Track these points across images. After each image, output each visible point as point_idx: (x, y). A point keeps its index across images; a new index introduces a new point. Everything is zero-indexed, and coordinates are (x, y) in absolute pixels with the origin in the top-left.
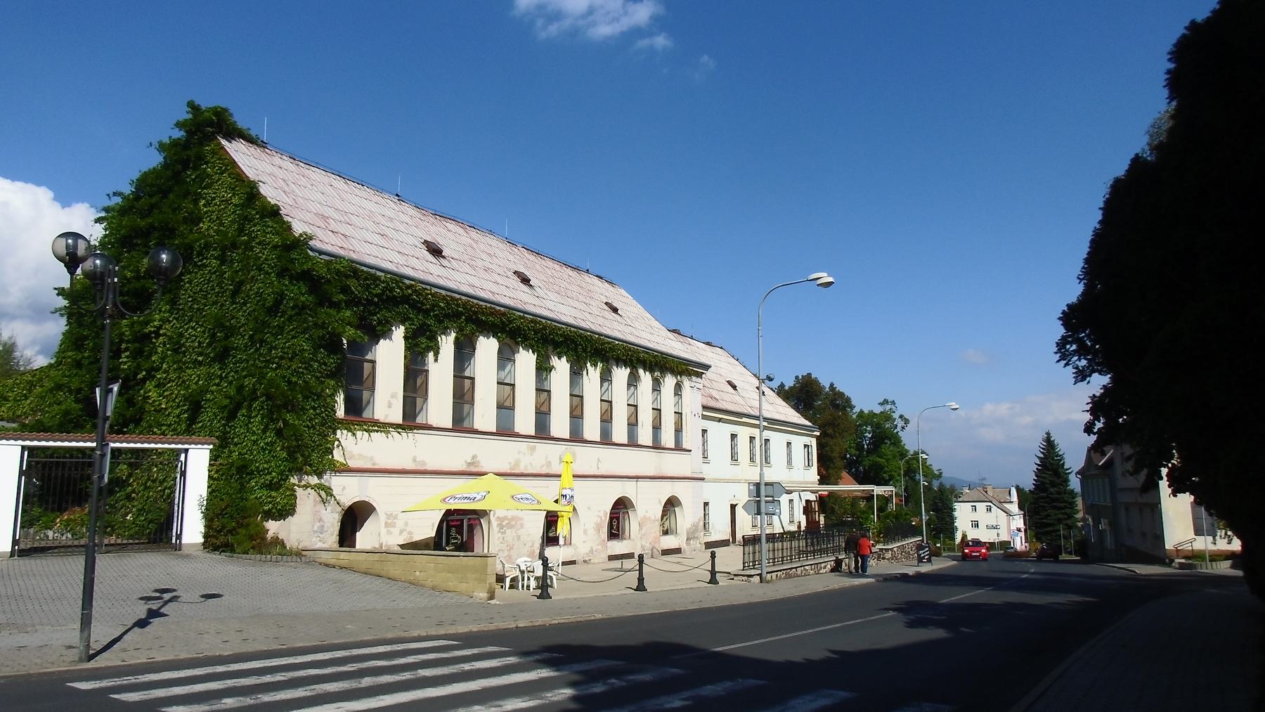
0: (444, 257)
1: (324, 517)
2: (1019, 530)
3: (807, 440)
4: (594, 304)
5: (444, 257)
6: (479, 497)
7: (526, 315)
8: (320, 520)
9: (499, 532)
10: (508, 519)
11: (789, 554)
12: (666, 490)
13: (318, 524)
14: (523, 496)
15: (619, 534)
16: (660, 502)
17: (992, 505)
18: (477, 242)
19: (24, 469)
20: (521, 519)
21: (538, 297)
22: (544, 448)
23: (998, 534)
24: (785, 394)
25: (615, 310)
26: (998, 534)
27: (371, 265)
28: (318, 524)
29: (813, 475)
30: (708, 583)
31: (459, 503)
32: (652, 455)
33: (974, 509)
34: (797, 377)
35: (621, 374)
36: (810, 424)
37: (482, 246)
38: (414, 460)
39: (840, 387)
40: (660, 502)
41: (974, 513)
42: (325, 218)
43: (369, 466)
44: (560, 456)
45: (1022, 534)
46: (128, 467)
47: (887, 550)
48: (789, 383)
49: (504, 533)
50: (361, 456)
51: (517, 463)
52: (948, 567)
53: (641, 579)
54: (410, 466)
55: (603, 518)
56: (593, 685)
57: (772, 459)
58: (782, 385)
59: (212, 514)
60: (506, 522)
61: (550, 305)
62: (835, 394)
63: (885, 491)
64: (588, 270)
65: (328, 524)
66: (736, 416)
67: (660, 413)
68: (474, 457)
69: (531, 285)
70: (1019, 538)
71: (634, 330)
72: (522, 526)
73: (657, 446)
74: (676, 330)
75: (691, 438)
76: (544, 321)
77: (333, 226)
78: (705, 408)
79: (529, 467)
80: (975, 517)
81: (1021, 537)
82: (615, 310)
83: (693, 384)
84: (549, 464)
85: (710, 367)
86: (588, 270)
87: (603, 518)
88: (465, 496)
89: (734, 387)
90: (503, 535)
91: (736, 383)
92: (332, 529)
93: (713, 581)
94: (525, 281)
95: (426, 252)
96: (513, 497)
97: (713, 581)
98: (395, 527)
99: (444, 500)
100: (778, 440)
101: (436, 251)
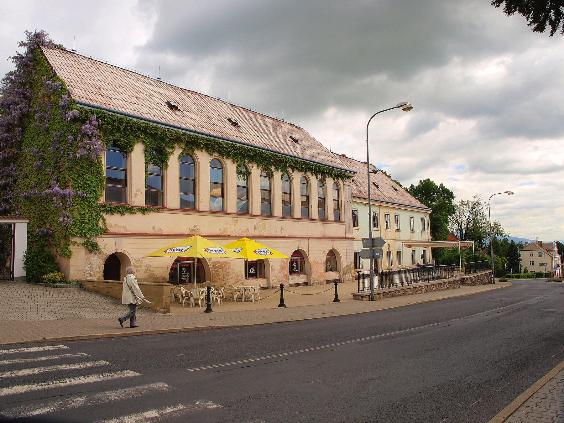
0: (179, 110)
1: (93, 262)
2: (558, 266)
3: (424, 216)
4: (282, 137)
5: (179, 110)
6: (185, 249)
7: (233, 143)
8: (90, 263)
12: (327, 246)
13: (89, 266)
14: (262, 250)
16: (324, 252)
17: (542, 252)
20: (229, 263)
22: (268, 222)
23: (546, 269)
25: (296, 141)
26: (546, 269)
27: (87, 105)
28: (89, 266)
29: (427, 236)
33: (531, 255)
35: (297, 176)
37: (210, 106)
38: (154, 228)
39: (446, 186)
40: (324, 252)
41: (531, 257)
42: (100, 88)
43: (123, 231)
44: (255, 225)
45: (560, 268)
46: (479, 257)
47: (467, 278)
50: (117, 226)
54: (151, 231)
55: (286, 262)
56: (104, 392)
57: (402, 227)
59: (29, 260)
60: (218, 264)
62: (443, 191)
63: (468, 245)
64: (283, 120)
67: (324, 200)
68: (195, 226)
70: (558, 270)
71: (307, 152)
72: (230, 267)
73: (323, 218)
74: (343, 155)
75: (347, 216)
76: (105, 112)
77: (104, 92)
79: (234, 232)
80: (532, 259)
81: (559, 270)
82: (296, 141)
86: (283, 120)
87: (286, 262)
90: (217, 273)
94: (235, 124)
99: (166, 251)
100: (404, 216)
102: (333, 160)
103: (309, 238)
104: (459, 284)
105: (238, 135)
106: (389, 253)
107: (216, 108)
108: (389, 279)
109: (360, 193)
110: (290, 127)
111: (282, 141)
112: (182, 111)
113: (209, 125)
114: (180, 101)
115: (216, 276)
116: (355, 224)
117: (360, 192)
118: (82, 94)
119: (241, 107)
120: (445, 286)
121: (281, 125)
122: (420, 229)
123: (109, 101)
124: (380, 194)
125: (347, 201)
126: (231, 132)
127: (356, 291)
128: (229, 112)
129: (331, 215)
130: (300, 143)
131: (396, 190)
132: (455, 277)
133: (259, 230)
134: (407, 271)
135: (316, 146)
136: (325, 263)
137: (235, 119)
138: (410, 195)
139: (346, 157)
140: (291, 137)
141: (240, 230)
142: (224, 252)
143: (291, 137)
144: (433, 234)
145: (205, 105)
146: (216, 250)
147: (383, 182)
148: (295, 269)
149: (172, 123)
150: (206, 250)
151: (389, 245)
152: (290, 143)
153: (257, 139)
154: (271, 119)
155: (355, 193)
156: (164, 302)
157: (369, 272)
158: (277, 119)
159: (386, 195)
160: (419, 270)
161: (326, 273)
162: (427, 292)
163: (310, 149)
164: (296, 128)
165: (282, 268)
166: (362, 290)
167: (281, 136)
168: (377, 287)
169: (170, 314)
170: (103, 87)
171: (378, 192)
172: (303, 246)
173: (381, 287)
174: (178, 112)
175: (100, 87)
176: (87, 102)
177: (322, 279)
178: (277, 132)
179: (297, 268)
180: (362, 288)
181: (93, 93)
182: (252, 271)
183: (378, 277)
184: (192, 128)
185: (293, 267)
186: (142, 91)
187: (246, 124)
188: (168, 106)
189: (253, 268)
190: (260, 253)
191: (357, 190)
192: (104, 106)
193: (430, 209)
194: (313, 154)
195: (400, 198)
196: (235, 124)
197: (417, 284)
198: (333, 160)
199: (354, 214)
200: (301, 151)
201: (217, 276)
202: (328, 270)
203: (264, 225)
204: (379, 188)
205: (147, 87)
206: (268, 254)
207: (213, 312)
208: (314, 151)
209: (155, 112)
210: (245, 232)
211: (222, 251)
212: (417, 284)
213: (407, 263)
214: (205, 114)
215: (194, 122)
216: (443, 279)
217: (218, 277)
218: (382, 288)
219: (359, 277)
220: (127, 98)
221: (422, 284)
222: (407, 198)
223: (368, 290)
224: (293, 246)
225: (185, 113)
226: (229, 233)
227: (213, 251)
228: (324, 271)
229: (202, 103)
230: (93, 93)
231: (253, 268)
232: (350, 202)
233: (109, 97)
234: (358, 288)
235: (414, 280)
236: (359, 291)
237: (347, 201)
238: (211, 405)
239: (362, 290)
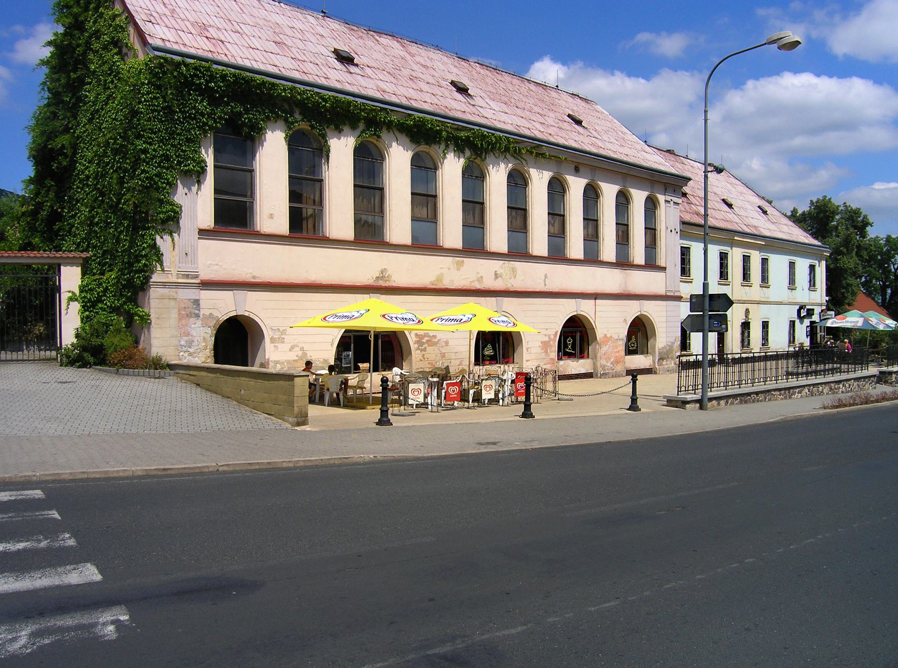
0: (357, 65)
5: (357, 65)
6: (465, 319)
9: (418, 349)
10: (429, 336)
11: (762, 376)
15: (575, 353)
18: (412, 55)
19: (58, 294)
21: (473, 105)
22: (521, 266)
24: (797, 219)
25: (579, 122)
30: (628, 409)
31: (450, 325)
32: (617, 273)
34: (811, 201)
36: (820, 244)
37: (418, 59)
42: (204, 27)
47: (891, 373)
48: (803, 208)
49: (425, 350)
51: (440, 278)
52: (45, 589)
53: (634, 399)
57: (807, 271)
58: (794, 211)
60: (427, 339)
61: (488, 113)
64: (557, 86)
65: (199, 339)
66: (729, 236)
69: (469, 95)
71: (597, 141)
73: (623, 262)
74: (670, 150)
77: (213, 32)
78: (684, 223)
82: (579, 122)
83: (669, 198)
84: (480, 279)
85: (690, 179)
86: (557, 86)
88: (452, 318)
89: (730, 206)
90: (423, 353)
91: (730, 200)
92: (204, 344)
93: (634, 407)
94: (462, 90)
95: (336, 61)
96: (489, 319)
97: (634, 407)
98: (283, 342)
100: (778, 263)
101: (345, 59)
102: (648, 156)
103: (596, 296)
104: (873, 383)
105: (467, 110)
106: (746, 326)
107: (429, 64)
108: (740, 372)
109: (696, 216)
110: (570, 99)
111: (550, 121)
112: (362, 66)
113: (411, 91)
114: (359, 50)
115: (422, 359)
116: (685, 271)
117: (697, 215)
118: (170, 35)
119: (478, 63)
120: (847, 386)
121: (554, 94)
122: (806, 285)
123: (221, 49)
124: (736, 219)
125: (671, 231)
126: (455, 105)
127: (672, 392)
128: (455, 70)
129: (638, 254)
130: (585, 126)
131: (765, 212)
132: (868, 369)
133: (503, 279)
134: (777, 357)
135: (618, 131)
136: (625, 339)
137: (465, 81)
138: (791, 223)
139: (674, 154)
140: (569, 116)
141: (468, 278)
142: (419, 321)
143: (569, 116)
144: (830, 290)
145: (408, 57)
146: (403, 318)
147: (742, 198)
148: (570, 349)
149: (338, 86)
150: (384, 316)
151: (746, 310)
152: (566, 126)
153: (504, 117)
154: (533, 83)
155: (687, 218)
156: (295, 405)
157: (700, 358)
158: (547, 85)
159: (748, 221)
160: (799, 355)
161: (626, 357)
162: (812, 395)
163: (605, 138)
164: (580, 101)
165: (545, 345)
166: (717, 387)
167: (552, 115)
168: (744, 382)
169: (306, 428)
170: (212, 23)
171: (730, 216)
172: (585, 308)
173: (736, 383)
174: (353, 69)
175: (207, 23)
176: (176, 47)
177: (619, 368)
178: (544, 106)
179: (574, 348)
180: (685, 387)
181: (191, 33)
182: (489, 351)
183: (725, 366)
184: (378, 95)
185: (566, 346)
186: (289, 32)
187: (485, 92)
188: (335, 58)
189: (489, 346)
190: (497, 322)
191: (691, 211)
192: (210, 55)
193: (827, 248)
194: (610, 146)
195: (773, 227)
196: (462, 90)
197: (793, 382)
198: (648, 156)
199: (683, 254)
200: (587, 140)
201: (424, 359)
202: (630, 351)
203: (514, 271)
204: (733, 208)
205: (298, 25)
206: (509, 325)
207: (392, 425)
208: (613, 140)
209: (309, 68)
210: (476, 282)
211: (415, 319)
212: (793, 382)
213: (779, 342)
214: (406, 72)
215: (383, 85)
216: (844, 372)
217: (426, 359)
218: (724, 386)
219: (685, 366)
220: (256, 43)
221: (803, 381)
222: (785, 229)
223: (697, 389)
224: (567, 309)
225: (369, 71)
226: (447, 284)
227: (398, 318)
228: (623, 353)
229: (403, 53)
230: (191, 33)
231: (489, 346)
232: (677, 232)
233: (223, 42)
234: (678, 387)
235: (788, 374)
236: (678, 392)
237: (671, 231)
238: (791, 547)
239: (685, 391)
